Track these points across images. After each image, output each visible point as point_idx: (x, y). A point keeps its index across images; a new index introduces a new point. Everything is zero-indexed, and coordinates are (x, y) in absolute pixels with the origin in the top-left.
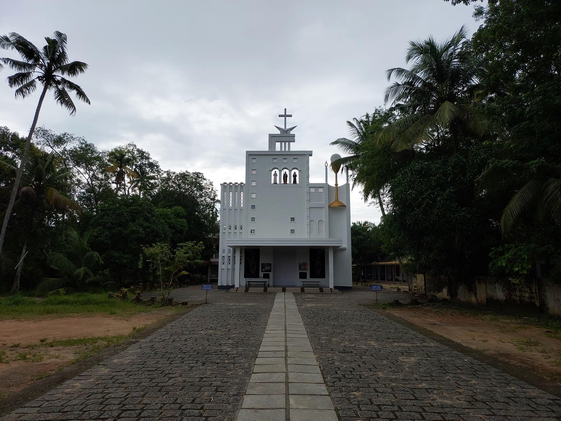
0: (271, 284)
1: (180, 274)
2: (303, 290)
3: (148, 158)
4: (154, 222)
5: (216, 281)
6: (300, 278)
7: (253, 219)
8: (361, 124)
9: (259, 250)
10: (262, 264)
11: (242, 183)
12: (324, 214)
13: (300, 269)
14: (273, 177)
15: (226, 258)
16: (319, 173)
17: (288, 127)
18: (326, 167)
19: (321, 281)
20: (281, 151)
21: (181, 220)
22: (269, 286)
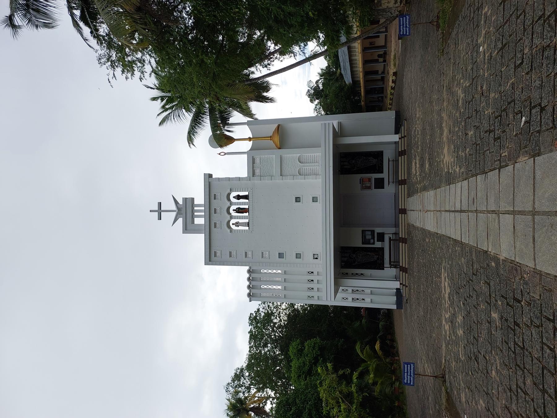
0: (393, 230)
1: (380, 353)
2: (403, 182)
3: (242, 370)
4: (303, 403)
6: (383, 187)
7: (298, 256)
8: (167, 107)
9: (343, 248)
10: (363, 243)
11: (249, 271)
12: (291, 155)
13: (369, 188)
14: (241, 228)
15: (356, 296)
16: (232, 164)
17: (174, 208)
19: (388, 155)
20: (205, 216)
21: (307, 347)
22: (396, 234)
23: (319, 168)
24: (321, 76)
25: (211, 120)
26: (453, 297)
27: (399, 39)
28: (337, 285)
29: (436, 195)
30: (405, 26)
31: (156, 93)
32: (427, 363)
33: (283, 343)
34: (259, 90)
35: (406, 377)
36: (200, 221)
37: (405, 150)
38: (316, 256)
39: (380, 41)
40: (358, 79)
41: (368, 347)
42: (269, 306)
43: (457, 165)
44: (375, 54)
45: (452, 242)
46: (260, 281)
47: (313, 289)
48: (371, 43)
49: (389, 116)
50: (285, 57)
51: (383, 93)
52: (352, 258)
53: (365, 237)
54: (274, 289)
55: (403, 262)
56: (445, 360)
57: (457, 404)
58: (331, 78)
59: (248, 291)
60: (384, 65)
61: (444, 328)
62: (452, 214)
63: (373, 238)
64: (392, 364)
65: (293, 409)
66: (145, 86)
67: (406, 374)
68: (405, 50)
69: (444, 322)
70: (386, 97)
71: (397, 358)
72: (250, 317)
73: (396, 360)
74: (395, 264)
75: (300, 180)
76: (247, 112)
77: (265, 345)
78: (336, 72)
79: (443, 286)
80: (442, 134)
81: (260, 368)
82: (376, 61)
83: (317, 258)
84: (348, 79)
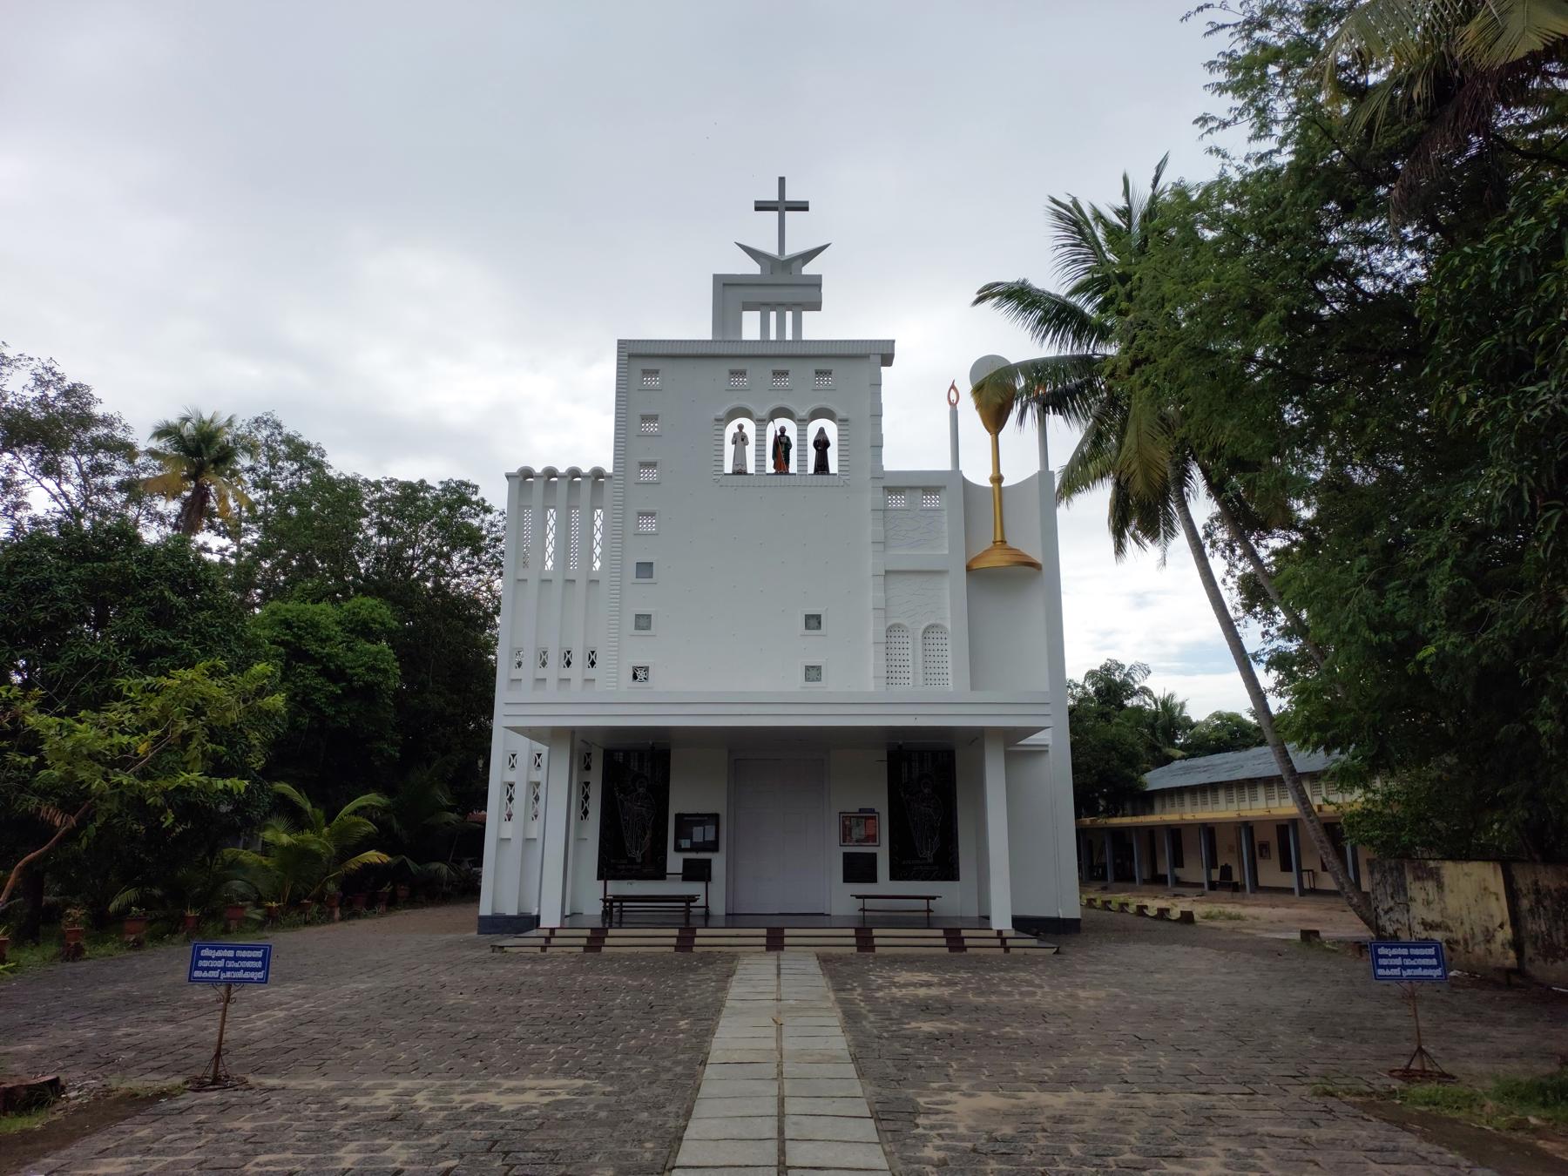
1: (353, 864)
2: (865, 941)
4: (197, 631)
5: (470, 890)
6: (848, 878)
7: (643, 622)
10: (679, 817)
11: (598, 473)
12: (948, 601)
13: (846, 836)
14: (729, 449)
17: (792, 249)
18: (953, 405)
19: (949, 897)
20: (765, 341)
23: (911, 686)
24: (1164, 704)
25: (1058, 360)
26: (482, 1126)
27: (1303, 932)
28: (553, 736)
29: (835, 1060)
30: (1408, 962)
31: (1142, 193)
32: (286, 1019)
33: (392, 583)
34: (1142, 513)
35: (219, 953)
36: (751, 327)
37: (964, 948)
38: (641, 674)
39: (1270, 873)
40: (1157, 806)
41: (371, 828)
42: (498, 540)
43: (947, 1148)
44: (1236, 859)
45: (672, 1123)
46: (569, 508)
47: (544, 664)
48: (1265, 847)
49: (1065, 899)
50: (1235, 591)
51: (1118, 879)
52: (636, 785)
53: (699, 823)
54: (545, 550)
55: (618, 938)
56: (272, 1089)
57: (99, 1141)
58: (1159, 735)
59: (538, 470)
60: (1201, 885)
61: (383, 1086)
62: (769, 1128)
63: (695, 848)
64: (319, 899)
65: (180, 601)
66: (1164, 161)
67: (230, 953)
68: (1275, 951)
69: (403, 1084)
70: (1104, 889)
71: (337, 914)
72: (467, 485)
73: (332, 913)
74: (614, 910)
75: (872, 630)
76: (1075, 480)
77: (384, 530)
78: (1174, 745)
79: (528, 1083)
80: (1041, 1084)
81: (319, 514)
82: (1212, 862)
83: (635, 677)
84: (1155, 779)
